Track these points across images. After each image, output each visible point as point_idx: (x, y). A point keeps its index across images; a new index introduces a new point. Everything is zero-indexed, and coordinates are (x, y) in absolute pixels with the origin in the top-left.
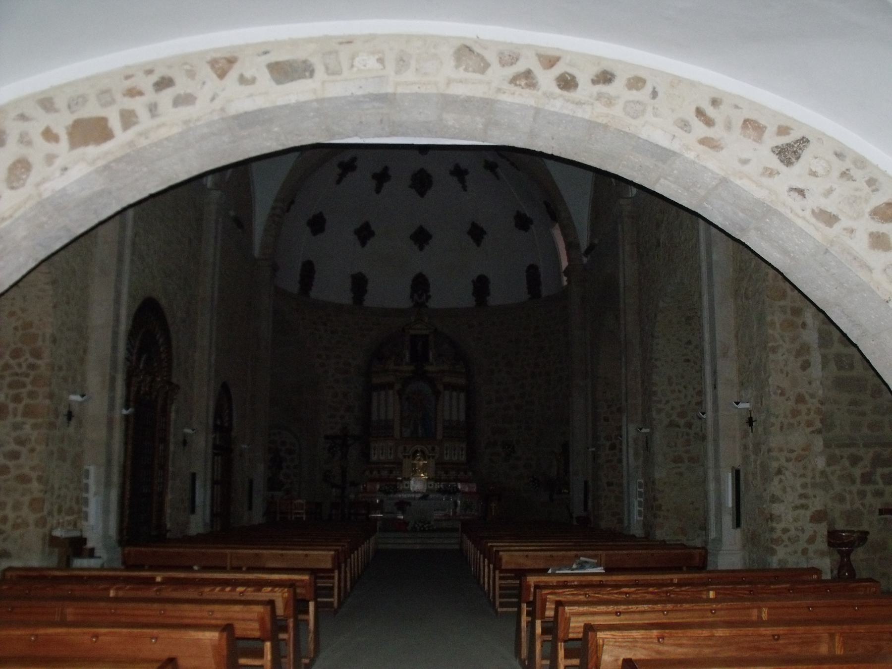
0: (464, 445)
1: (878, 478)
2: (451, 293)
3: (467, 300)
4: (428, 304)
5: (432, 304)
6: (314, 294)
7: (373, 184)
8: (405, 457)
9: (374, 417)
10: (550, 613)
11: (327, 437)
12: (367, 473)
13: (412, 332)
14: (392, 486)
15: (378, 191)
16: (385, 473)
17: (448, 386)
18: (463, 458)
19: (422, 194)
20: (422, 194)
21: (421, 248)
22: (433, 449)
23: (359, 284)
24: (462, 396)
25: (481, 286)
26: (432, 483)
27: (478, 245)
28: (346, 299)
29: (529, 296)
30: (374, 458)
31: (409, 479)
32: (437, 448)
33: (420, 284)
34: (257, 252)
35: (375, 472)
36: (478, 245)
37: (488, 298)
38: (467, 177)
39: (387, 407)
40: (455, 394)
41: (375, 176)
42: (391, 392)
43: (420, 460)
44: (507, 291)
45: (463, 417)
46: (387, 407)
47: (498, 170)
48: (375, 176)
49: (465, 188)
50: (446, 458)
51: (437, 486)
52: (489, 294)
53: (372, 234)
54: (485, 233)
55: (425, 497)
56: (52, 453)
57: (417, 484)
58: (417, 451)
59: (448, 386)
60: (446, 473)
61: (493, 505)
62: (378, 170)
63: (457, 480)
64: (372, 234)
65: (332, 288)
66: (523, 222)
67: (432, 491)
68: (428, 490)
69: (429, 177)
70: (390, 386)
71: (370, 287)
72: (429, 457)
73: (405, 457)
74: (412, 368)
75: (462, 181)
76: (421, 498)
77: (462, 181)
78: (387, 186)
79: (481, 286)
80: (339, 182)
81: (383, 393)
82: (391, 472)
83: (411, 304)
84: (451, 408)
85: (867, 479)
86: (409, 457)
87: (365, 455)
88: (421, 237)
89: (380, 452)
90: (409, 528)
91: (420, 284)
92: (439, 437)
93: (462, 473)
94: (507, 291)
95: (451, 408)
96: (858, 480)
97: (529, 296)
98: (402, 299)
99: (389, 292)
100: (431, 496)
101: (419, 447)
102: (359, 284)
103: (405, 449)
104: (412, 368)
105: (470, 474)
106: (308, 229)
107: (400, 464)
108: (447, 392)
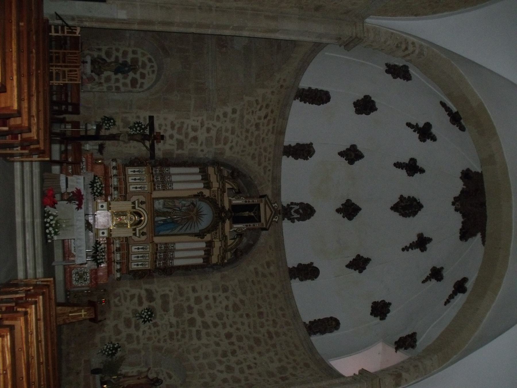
0: (148, 267)
2: (298, 242)
4: (286, 219)
5: (286, 224)
6: (297, 105)
7: (406, 160)
8: (134, 203)
9: (173, 170)
10: (7, 323)
11: (151, 118)
12: (114, 164)
14: (101, 191)
15: (398, 165)
16: (115, 182)
17: (210, 244)
18: (133, 266)
19: (395, 208)
20: (395, 208)
21: (338, 211)
22: (143, 234)
23: (303, 151)
24: (200, 261)
25: (308, 272)
26: (106, 235)
27: (348, 266)
28: (291, 138)
29: (307, 323)
30: (130, 171)
31: (109, 209)
32: (143, 238)
33: (306, 212)
34: (371, 21)
35: (115, 172)
36: (348, 266)
37: (297, 279)
38: (418, 251)
39: (185, 182)
40: (202, 253)
41: (413, 161)
42: (201, 185)
43: (131, 219)
44: (310, 300)
45: (177, 263)
46: (185, 182)
47: (434, 281)
48: (413, 161)
50: (133, 249)
51: (102, 240)
52: (301, 280)
53: (351, 162)
54: (360, 272)
55: (89, 226)
57: (103, 218)
58: (140, 216)
59: (210, 244)
60: (118, 250)
61: (83, 313)
62: (420, 164)
63: (110, 262)
64: (351, 162)
65: (301, 123)
67: (97, 235)
68: (98, 229)
69: (414, 214)
70: (208, 185)
71: (308, 283)
72: (135, 230)
73: (134, 203)
74: (227, 206)
75: (412, 246)
76: (87, 223)
77: (412, 246)
78: (403, 173)
79: (308, 272)
80: (409, 125)
81: (199, 177)
82: (116, 188)
83: (285, 205)
84: (187, 250)
86: (134, 208)
87: (136, 162)
88: (349, 210)
89: (136, 179)
90: (48, 208)
91: (306, 212)
92: (157, 240)
93: (118, 267)
94: (310, 300)
95: (187, 250)
97: (307, 323)
99: (295, 182)
100: (91, 234)
101: (145, 218)
102: (303, 151)
103: (142, 203)
104: (227, 206)
105: (118, 275)
106: (361, 97)
107: (125, 198)
108: (203, 245)
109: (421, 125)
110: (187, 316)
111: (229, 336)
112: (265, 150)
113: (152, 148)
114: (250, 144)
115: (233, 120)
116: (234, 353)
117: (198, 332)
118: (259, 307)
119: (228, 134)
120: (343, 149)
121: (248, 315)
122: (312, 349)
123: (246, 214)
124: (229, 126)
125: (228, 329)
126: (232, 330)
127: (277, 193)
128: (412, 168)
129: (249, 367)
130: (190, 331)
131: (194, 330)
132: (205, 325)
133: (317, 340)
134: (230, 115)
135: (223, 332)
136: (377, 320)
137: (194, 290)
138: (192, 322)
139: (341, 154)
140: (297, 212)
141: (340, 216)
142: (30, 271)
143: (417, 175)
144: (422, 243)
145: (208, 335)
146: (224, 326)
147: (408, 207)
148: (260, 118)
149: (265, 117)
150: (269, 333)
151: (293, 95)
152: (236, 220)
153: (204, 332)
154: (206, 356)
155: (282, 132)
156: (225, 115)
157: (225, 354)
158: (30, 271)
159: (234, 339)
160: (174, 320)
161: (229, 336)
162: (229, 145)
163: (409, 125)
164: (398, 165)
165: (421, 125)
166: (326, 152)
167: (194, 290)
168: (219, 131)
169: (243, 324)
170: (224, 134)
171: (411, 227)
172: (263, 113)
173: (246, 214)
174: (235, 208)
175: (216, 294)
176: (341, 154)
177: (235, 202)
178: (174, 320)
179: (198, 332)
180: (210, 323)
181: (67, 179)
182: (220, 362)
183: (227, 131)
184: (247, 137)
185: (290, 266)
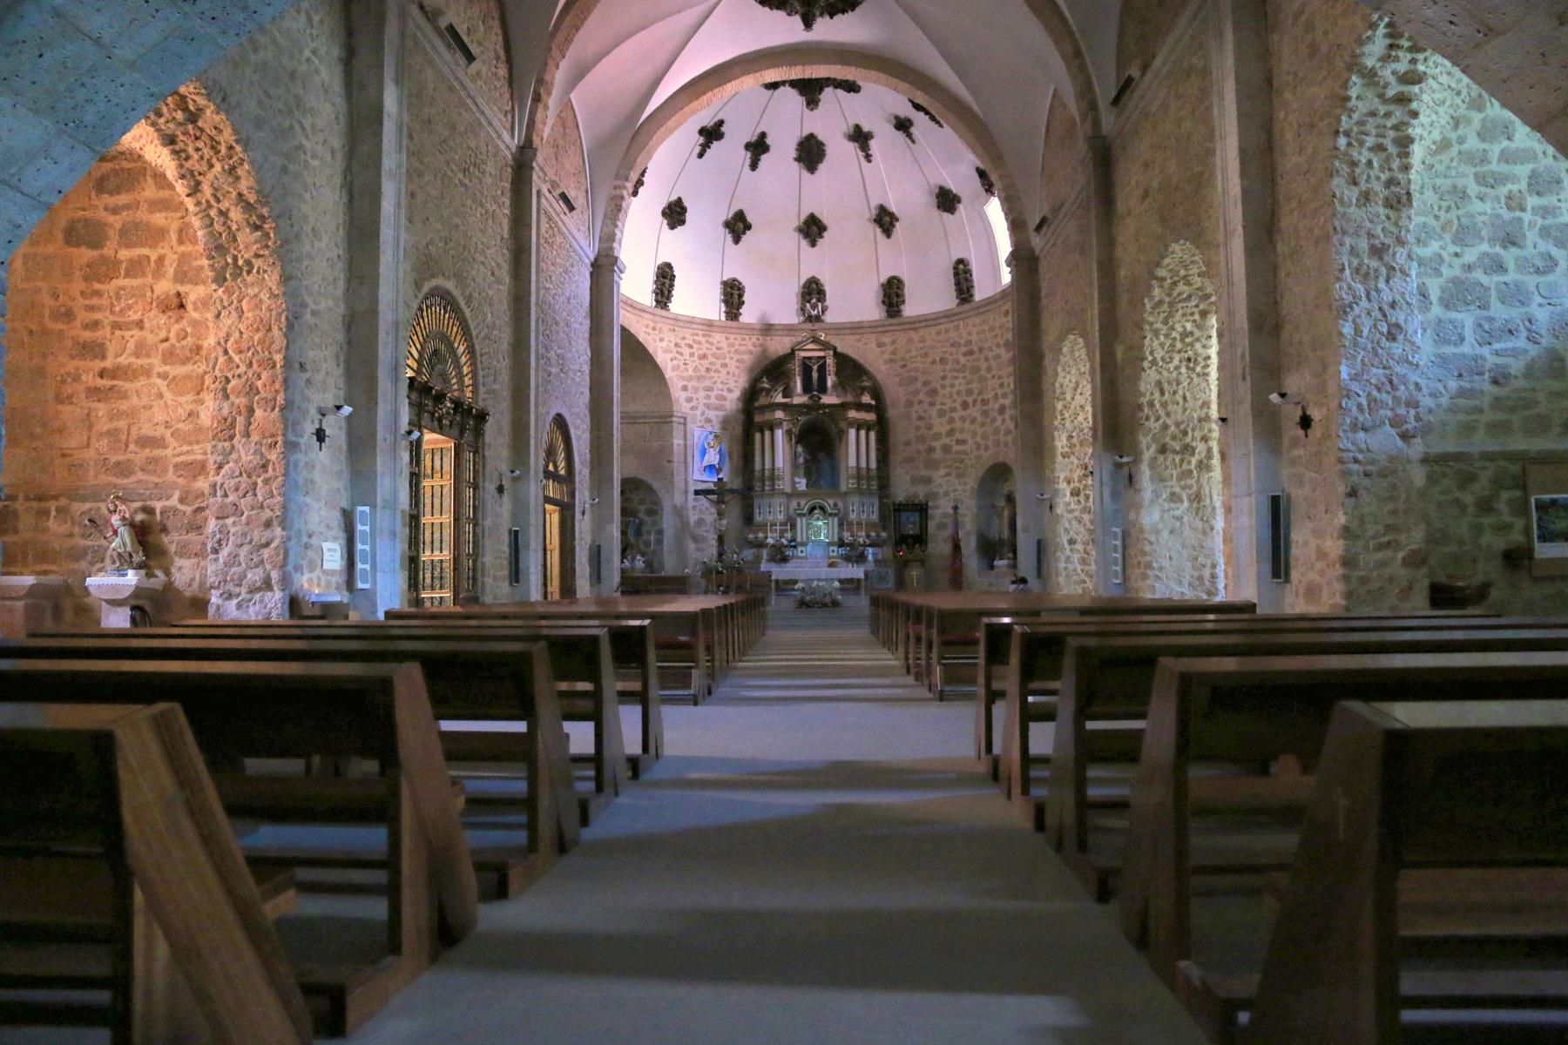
1: (1502, 506)
3: (871, 310)
13: (803, 354)
15: (754, 166)
19: (812, 169)
20: (812, 169)
25: (892, 293)
27: (889, 236)
33: (813, 291)
36: (889, 236)
38: (872, 143)
48: (748, 146)
49: (868, 158)
53: (728, 225)
56: (990, 549)
66: (947, 201)
71: (907, 292)
75: (865, 148)
77: (865, 148)
78: (765, 159)
79: (892, 293)
85: (1486, 506)
91: (813, 291)
94: (928, 297)
96: (1471, 510)
98: (787, 312)
109: (702, 140)
110: (938, 455)
111: (965, 405)
112: (733, 345)
113: (732, 491)
114: (725, 365)
115: (696, 390)
116: (985, 402)
117: (959, 442)
118: (934, 362)
119: (713, 394)
120: (729, 238)
121: (943, 378)
122: (990, 302)
123: (815, 375)
124: (702, 394)
125: (957, 405)
126: (959, 400)
127: (789, 329)
128: (758, 147)
129: (1001, 385)
130: (957, 452)
131: (955, 448)
132: (951, 432)
133: (980, 294)
134: (688, 394)
135: (961, 413)
136: (961, 208)
137: (908, 443)
138: (946, 449)
139: (737, 240)
140: (814, 307)
141: (820, 242)
142: (863, 464)
143: (768, 141)
144: (860, 137)
145: (962, 430)
146: (953, 410)
147: (810, 153)
148: (692, 355)
149: (691, 347)
150: (965, 354)
151: (663, 313)
152: (823, 389)
153: (958, 436)
154: (985, 437)
155: (709, 324)
156: (689, 400)
157: (985, 414)
158: (863, 464)
159: (970, 400)
160: (942, 472)
161: (965, 405)
162: (725, 393)
163: (701, 155)
164: (754, 166)
165: (702, 140)
166: (738, 262)
167: (908, 443)
168: (708, 407)
169: (953, 386)
170: (713, 400)
171: (839, 150)
172: (687, 351)
173: (815, 375)
174: (807, 388)
175: (915, 416)
176: (737, 240)
177: (799, 388)
178: (942, 472)
179: (959, 442)
180: (948, 427)
181: (1278, 562)
182: (994, 420)
183: (708, 397)
184: (717, 371)
185: (884, 315)
